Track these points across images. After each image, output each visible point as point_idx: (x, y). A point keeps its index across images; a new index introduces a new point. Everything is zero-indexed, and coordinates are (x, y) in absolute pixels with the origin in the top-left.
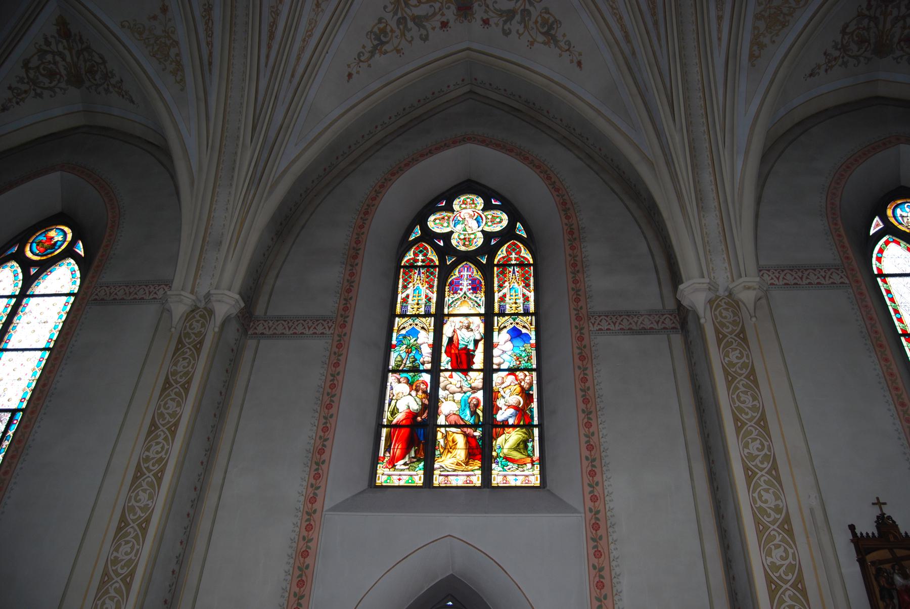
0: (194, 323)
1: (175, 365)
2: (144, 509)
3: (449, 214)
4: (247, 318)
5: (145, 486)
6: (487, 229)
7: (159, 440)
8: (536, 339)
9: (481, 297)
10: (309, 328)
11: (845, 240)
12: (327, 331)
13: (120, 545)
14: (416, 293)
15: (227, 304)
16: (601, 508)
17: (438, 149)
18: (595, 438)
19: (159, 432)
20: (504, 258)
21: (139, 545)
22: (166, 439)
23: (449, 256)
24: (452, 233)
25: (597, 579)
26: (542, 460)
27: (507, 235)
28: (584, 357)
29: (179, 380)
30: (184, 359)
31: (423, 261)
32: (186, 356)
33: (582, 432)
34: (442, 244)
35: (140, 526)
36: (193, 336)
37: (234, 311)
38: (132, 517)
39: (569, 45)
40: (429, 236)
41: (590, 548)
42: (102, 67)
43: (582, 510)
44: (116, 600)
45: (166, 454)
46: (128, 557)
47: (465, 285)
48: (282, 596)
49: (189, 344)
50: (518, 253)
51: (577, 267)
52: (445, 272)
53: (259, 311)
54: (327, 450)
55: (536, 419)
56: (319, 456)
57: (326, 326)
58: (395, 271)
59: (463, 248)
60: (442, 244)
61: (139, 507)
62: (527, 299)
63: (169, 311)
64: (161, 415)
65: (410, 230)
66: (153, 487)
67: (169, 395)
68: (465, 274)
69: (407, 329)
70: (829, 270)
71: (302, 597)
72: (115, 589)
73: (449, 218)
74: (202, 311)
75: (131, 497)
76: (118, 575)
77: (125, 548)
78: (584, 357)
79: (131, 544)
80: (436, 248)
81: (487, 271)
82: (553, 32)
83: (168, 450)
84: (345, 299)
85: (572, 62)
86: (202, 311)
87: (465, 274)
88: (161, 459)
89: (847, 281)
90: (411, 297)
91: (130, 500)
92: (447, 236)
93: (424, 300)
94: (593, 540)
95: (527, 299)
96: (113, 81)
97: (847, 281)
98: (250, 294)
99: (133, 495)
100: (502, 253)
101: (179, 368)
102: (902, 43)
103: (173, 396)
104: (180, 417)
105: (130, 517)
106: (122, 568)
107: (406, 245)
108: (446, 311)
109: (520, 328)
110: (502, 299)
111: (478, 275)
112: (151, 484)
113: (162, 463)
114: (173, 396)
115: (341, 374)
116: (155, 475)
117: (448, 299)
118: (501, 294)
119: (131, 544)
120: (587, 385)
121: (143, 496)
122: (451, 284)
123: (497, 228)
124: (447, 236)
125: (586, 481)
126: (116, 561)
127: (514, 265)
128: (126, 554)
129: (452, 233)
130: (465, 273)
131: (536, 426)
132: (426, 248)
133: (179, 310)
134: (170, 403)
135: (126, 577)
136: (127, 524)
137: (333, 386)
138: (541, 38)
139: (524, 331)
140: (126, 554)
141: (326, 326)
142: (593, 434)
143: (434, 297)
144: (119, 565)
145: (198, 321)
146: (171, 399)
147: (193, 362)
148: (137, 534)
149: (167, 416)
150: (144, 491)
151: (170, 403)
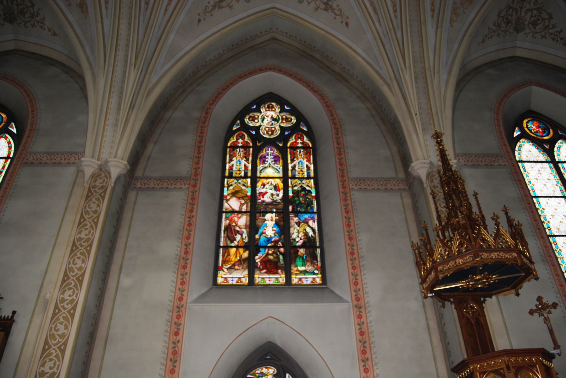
0: (92, 204)
1: (63, 293)
2: (80, 269)
3: (258, 114)
4: (130, 180)
5: (79, 255)
6: (282, 125)
7: (87, 227)
8: (317, 209)
9: (280, 166)
10: (171, 185)
11: (502, 129)
12: (183, 186)
13: (45, 362)
14: (239, 163)
15: (118, 167)
16: (367, 339)
17: (251, 74)
18: (353, 233)
19: (86, 222)
20: (293, 142)
21: (59, 361)
22: (92, 227)
23: (258, 144)
24: (260, 126)
25: (362, 349)
26: (319, 213)
27: (295, 129)
28: (348, 211)
29: (66, 306)
30: (70, 289)
31: (242, 143)
32: (71, 286)
33: (346, 230)
34: (254, 133)
35: (59, 348)
36: (91, 213)
37: (124, 172)
38: (87, 216)
39: (341, 12)
40: (246, 128)
41: (357, 330)
42: (31, 9)
43: (350, 301)
44: (64, 324)
45: (57, 369)
46: (71, 298)
47: (270, 159)
48: (165, 335)
49: (73, 276)
50: (302, 140)
51: (340, 152)
52: (257, 150)
53: (139, 173)
54: (192, 237)
55: (318, 243)
56: (184, 263)
57: (182, 183)
58: (225, 151)
59: (267, 136)
60: (254, 133)
61: (58, 335)
62: (308, 168)
63: (83, 172)
64: (87, 213)
65: (233, 123)
66: (68, 321)
67: (91, 200)
68: (270, 152)
69: (234, 186)
70: (497, 157)
71: (180, 325)
72: (63, 317)
73: (258, 116)
74: (103, 170)
75: (51, 328)
76: (65, 309)
77: (49, 364)
78: (348, 211)
79: (53, 362)
80: (250, 135)
81: (283, 151)
82: (330, 3)
83: (59, 365)
84: (182, 275)
85: (342, 22)
86: (103, 170)
87: (270, 152)
88: (73, 300)
89: (507, 164)
90: (235, 166)
91: (69, 263)
92: (257, 129)
93: (243, 168)
94: (363, 361)
95: (308, 168)
96: (38, 19)
97: (507, 164)
98: (135, 159)
99: (53, 326)
100: (292, 140)
101: (66, 296)
102: (530, 25)
103: (62, 320)
104: (100, 213)
105: (70, 274)
106: (67, 304)
107: (230, 133)
108: (258, 175)
109: (305, 186)
110: (294, 168)
111: (276, 152)
112: (65, 318)
113: (90, 242)
114: (62, 320)
115: (195, 217)
116: (69, 312)
117: (260, 167)
118: (292, 164)
119: (53, 362)
120: (351, 228)
121: (61, 327)
122: (260, 158)
123: (289, 125)
124: (257, 129)
125: (349, 258)
126: (63, 300)
127: (300, 147)
128: (70, 296)
129: (260, 126)
130: (270, 152)
131: (318, 247)
132: (244, 136)
133: (88, 172)
134: (59, 326)
135: (87, 247)
136: (69, 278)
137: (186, 253)
138: (323, 6)
139: (308, 188)
140: (70, 296)
141: (182, 183)
142: (352, 231)
143: (250, 167)
144: (66, 303)
145: (94, 203)
146: (78, 258)
147: (92, 231)
148: (58, 354)
149: (57, 336)
150: (61, 323)
151: (92, 205)
